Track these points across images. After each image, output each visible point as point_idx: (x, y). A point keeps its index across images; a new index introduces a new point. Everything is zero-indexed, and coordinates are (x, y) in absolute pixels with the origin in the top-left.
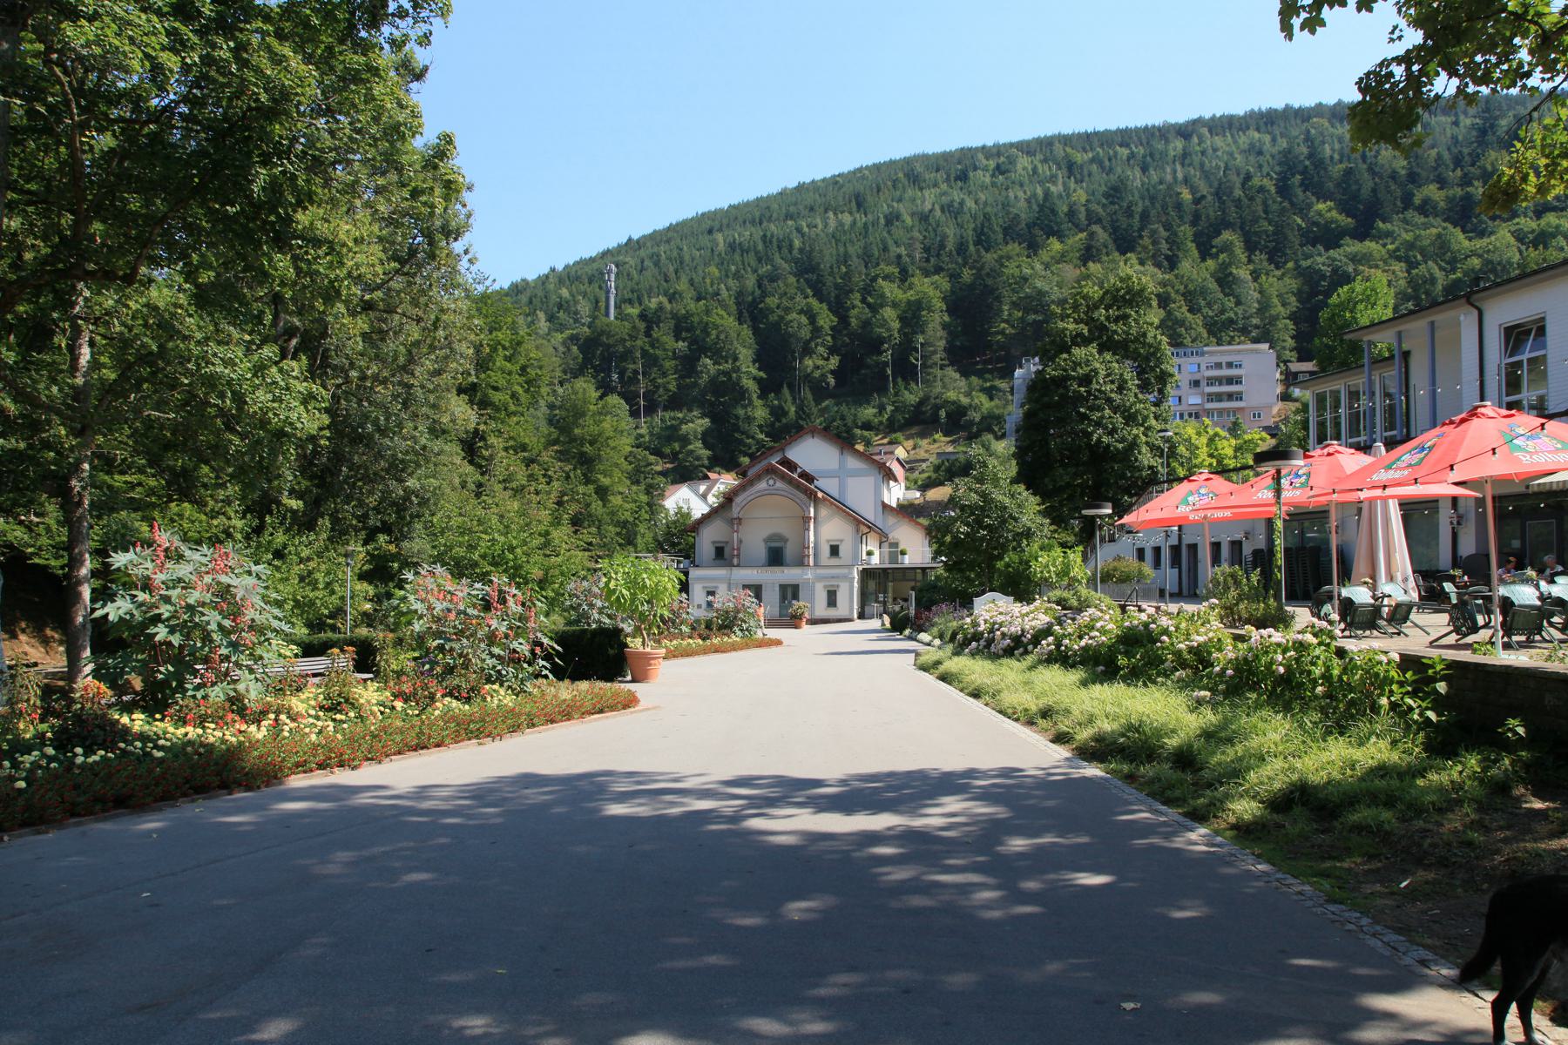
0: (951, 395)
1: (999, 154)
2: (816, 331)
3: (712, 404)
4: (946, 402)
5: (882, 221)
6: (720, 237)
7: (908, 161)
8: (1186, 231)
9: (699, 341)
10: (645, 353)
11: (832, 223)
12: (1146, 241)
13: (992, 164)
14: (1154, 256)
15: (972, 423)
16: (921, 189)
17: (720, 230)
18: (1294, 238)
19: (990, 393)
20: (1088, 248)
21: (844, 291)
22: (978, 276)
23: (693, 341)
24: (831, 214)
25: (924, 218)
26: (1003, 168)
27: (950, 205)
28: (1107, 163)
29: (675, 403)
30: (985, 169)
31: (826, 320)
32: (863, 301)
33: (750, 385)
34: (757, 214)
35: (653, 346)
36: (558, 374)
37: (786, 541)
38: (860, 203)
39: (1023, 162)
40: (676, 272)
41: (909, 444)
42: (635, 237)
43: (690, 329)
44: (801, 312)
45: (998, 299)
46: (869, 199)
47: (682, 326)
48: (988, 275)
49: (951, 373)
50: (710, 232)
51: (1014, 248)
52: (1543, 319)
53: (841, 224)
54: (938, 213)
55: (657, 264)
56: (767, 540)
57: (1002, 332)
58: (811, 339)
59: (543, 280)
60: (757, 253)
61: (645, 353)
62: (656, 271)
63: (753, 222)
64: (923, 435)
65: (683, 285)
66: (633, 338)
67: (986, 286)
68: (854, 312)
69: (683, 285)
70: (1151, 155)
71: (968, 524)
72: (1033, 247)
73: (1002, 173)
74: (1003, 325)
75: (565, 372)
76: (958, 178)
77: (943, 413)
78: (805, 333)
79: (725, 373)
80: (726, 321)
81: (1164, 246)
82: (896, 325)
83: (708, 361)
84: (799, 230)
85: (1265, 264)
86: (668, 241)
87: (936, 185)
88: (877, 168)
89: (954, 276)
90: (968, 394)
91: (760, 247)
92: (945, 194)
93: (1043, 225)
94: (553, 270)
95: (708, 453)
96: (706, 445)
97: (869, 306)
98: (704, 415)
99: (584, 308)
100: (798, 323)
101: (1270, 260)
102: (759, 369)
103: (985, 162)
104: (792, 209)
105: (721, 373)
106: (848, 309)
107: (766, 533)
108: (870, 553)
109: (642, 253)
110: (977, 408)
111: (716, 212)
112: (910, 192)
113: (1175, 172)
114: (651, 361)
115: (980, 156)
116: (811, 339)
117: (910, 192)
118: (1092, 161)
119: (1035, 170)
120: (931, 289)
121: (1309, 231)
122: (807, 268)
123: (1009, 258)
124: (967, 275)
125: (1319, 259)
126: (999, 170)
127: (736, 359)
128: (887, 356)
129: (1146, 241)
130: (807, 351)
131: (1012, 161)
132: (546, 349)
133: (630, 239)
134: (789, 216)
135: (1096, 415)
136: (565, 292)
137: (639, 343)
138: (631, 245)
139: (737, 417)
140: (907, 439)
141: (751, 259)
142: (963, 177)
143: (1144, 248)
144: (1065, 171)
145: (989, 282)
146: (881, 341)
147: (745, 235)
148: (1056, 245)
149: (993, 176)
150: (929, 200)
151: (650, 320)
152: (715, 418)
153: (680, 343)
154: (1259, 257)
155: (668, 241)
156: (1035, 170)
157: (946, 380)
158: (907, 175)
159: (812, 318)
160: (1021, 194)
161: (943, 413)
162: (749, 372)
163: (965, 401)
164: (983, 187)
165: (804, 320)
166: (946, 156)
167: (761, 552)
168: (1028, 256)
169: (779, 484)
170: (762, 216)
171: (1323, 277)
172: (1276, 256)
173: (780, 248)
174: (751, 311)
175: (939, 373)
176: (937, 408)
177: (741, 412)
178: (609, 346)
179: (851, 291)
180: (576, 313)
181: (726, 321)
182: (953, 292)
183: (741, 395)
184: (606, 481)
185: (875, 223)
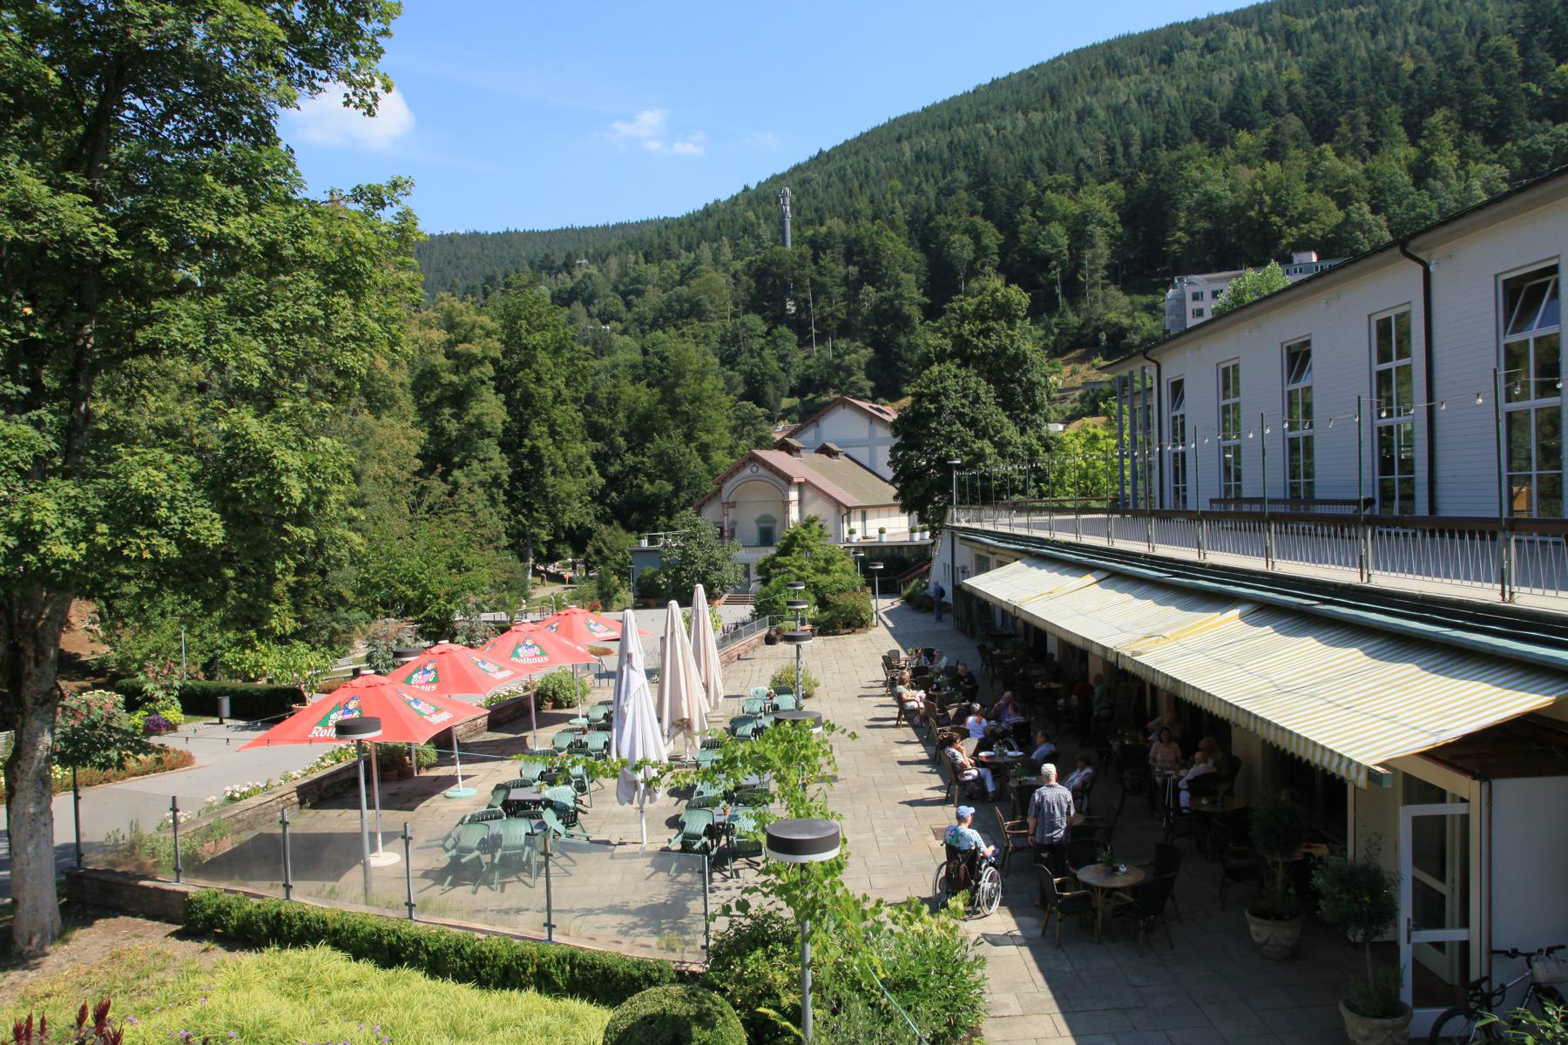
0: (1112, 316)
1: (1211, 28)
2: (980, 250)
3: (875, 333)
4: (1107, 323)
5: (1074, 118)
6: (906, 146)
7: (1109, 45)
8: (1394, 112)
9: (870, 268)
10: (813, 282)
11: (1021, 124)
12: (1344, 128)
13: (1201, 41)
14: (1353, 146)
15: (1131, 346)
16: (1121, 77)
17: (909, 137)
18: (1521, 109)
19: (1151, 309)
20: (1273, 143)
21: (1015, 203)
22: (1153, 182)
23: (864, 266)
24: (1020, 115)
25: (1116, 110)
26: (1213, 45)
27: (1146, 95)
28: (1331, 30)
29: (845, 330)
30: (1192, 49)
31: (992, 237)
32: (1033, 215)
33: (916, 313)
34: (947, 117)
35: (820, 274)
36: (730, 307)
37: (775, 521)
38: (1054, 96)
39: (1237, 36)
40: (861, 187)
41: (1067, 370)
42: (826, 149)
43: (862, 252)
44: (966, 231)
45: (1174, 206)
46: (1064, 92)
47: (852, 250)
48: (1163, 180)
49: (1113, 290)
50: (899, 140)
51: (1196, 147)
52: (1308, 343)
53: (1030, 124)
54: (1134, 105)
55: (843, 179)
56: (758, 521)
57: (1178, 241)
58: (976, 259)
59: (734, 200)
60: (942, 161)
61: (813, 282)
62: (841, 186)
63: (942, 127)
64: (1081, 360)
65: (862, 203)
66: (802, 266)
67: (1161, 192)
68: (1023, 228)
69: (862, 203)
70: (1384, 16)
71: (667, 576)
72: (1217, 143)
73: (1211, 51)
74: (1179, 234)
75: (736, 304)
76: (1162, 61)
77: (1103, 337)
78: (968, 254)
79: (890, 301)
80: (897, 247)
81: (1365, 133)
82: (1065, 241)
83: (871, 288)
84: (986, 133)
85: (1480, 146)
86: (857, 153)
87: (1137, 71)
88: (1078, 54)
89: (1129, 183)
90: (1129, 315)
91: (946, 155)
92: (1146, 81)
93: (1214, 130)
94: (746, 189)
95: (872, 384)
96: (869, 377)
97: (1039, 219)
98: (866, 346)
99: (765, 231)
100: (961, 245)
101: (1485, 142)
102: (924, 295)
103: (1192, 39)
104: (983, 110)
105: (883, 300)
106: (1018, 224)
107: (757, 515)
108: (852, 532)
109: (830, 167)
110: (1136, 330)
111: (906, 117)
112: (1107, 81)
113: (1406, 34)
114: (819, 289)
115: (1187, 33)
116: (976, 259)
117: (1107, 81)
118: (1314, 28)
119: (1247, 45)
120: (1099, 200)
121: (1547, 99)
122: (981, 180)
123: (1188, 158)
124: (1143, 180)
125: (1541, 138)
126: (1209, 48)
127: (898, 285)
128: (1056, 274)
129: (1344, 128)
130: (973, 272)
131: (1222, 37)
132: (719, 284)
133: (821, 152)
134: (980, 118)
135: (944, 430)
136: (751, 215)
137: (807, 271)
138: (822, 159)
139: (899, 346)
140: (1067, 363)
141: (936, 169)
142: (1167, 59)
143: (1344, 136)
144: (1282, 44)
145: (1164, 187)
146: (1047, 259)
147: (931, 142)
148: (1244, 137)
149: (1202, 55)
150: (1124, 90)
151: (818, 246)
152: (875, 343)
153: (851, 268)
154: (1474, 140)
155: (857, 153)
156: (1247, 45)
157: (1109, 300)
158: (1108, 63)
159: (976, 236)
160: (1226, 77)
161: (1103, 337)
162: (912, 294)
163: (1126, 322)
164: (1188, 70)
165: (966, 239)
166: (1151, 36)
167: (753, 533)
168: (1210, 156)
169: (762, 471)
170: (952, 119)
171: (1544, 158)
172: (1494, 137)
173: (965, 154)
174: (924, 234)
175: (1099, 292)
176: (1098, 330)
177: (903, 340)
178: (780, 276)
179: (1021, 205)
180: (758, 237)
181: (897, 247)
182: (1128, 200)
183: (904, 323)
184: (706, 438)
185: (1067, 120)
